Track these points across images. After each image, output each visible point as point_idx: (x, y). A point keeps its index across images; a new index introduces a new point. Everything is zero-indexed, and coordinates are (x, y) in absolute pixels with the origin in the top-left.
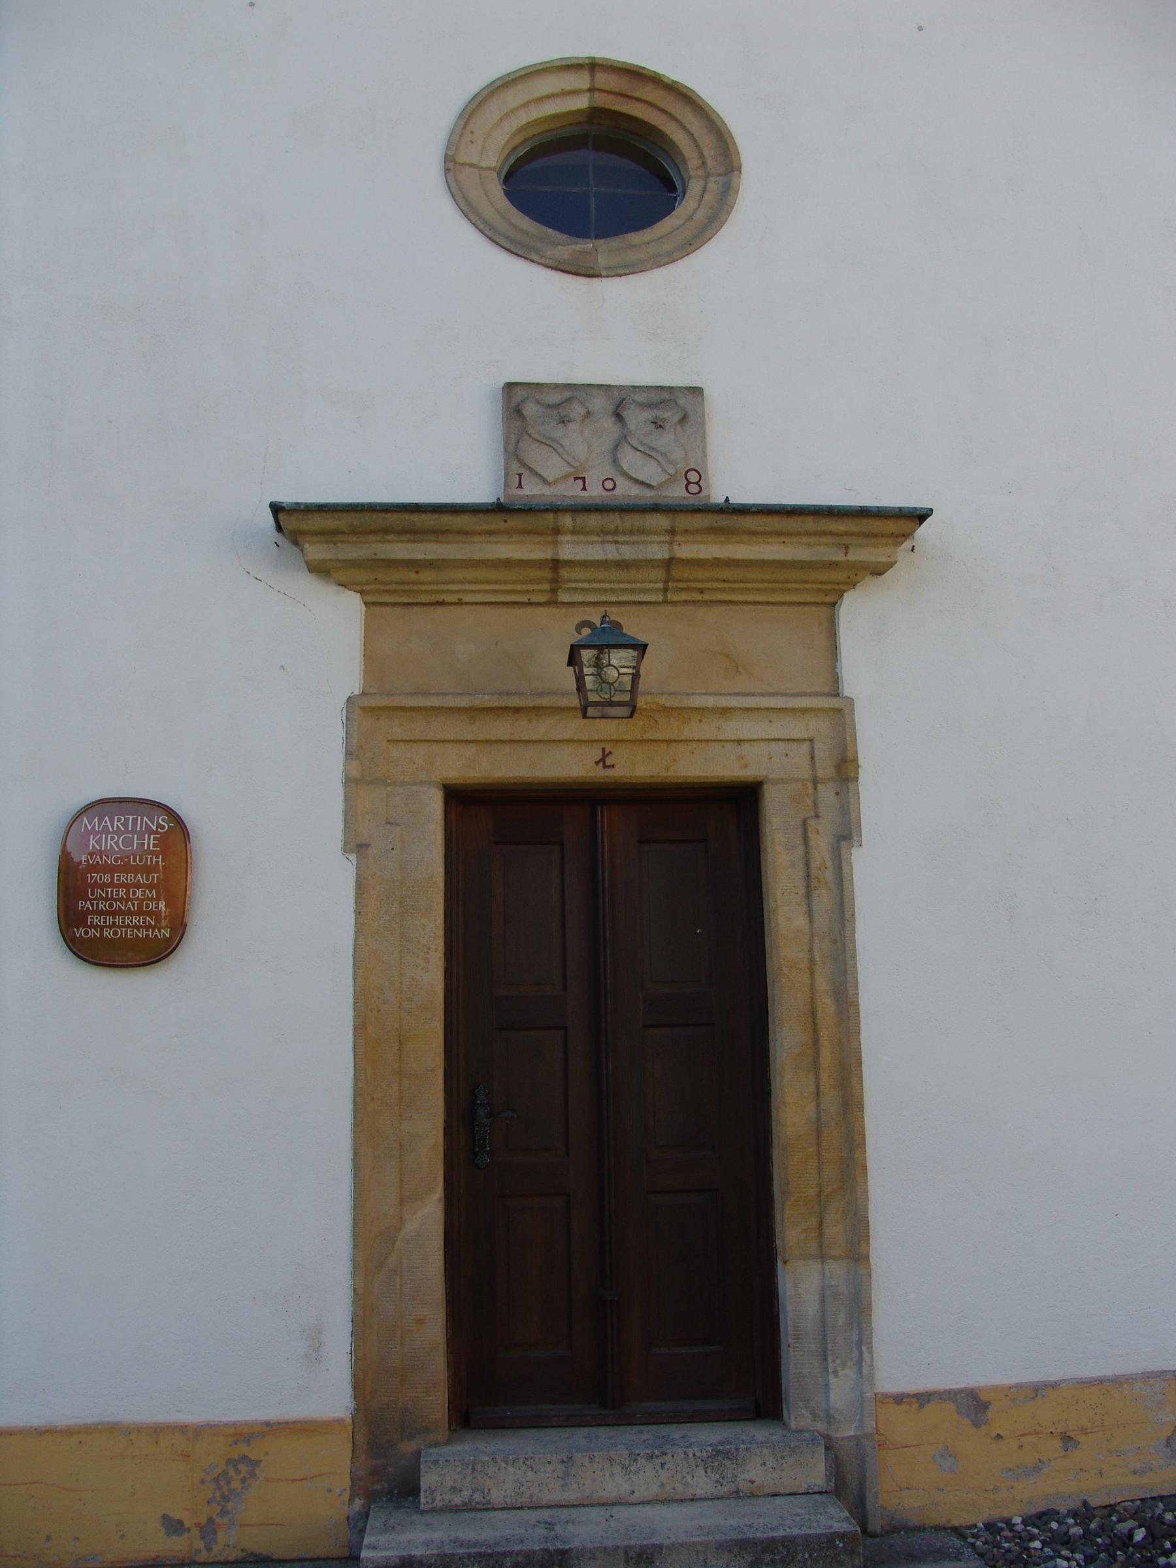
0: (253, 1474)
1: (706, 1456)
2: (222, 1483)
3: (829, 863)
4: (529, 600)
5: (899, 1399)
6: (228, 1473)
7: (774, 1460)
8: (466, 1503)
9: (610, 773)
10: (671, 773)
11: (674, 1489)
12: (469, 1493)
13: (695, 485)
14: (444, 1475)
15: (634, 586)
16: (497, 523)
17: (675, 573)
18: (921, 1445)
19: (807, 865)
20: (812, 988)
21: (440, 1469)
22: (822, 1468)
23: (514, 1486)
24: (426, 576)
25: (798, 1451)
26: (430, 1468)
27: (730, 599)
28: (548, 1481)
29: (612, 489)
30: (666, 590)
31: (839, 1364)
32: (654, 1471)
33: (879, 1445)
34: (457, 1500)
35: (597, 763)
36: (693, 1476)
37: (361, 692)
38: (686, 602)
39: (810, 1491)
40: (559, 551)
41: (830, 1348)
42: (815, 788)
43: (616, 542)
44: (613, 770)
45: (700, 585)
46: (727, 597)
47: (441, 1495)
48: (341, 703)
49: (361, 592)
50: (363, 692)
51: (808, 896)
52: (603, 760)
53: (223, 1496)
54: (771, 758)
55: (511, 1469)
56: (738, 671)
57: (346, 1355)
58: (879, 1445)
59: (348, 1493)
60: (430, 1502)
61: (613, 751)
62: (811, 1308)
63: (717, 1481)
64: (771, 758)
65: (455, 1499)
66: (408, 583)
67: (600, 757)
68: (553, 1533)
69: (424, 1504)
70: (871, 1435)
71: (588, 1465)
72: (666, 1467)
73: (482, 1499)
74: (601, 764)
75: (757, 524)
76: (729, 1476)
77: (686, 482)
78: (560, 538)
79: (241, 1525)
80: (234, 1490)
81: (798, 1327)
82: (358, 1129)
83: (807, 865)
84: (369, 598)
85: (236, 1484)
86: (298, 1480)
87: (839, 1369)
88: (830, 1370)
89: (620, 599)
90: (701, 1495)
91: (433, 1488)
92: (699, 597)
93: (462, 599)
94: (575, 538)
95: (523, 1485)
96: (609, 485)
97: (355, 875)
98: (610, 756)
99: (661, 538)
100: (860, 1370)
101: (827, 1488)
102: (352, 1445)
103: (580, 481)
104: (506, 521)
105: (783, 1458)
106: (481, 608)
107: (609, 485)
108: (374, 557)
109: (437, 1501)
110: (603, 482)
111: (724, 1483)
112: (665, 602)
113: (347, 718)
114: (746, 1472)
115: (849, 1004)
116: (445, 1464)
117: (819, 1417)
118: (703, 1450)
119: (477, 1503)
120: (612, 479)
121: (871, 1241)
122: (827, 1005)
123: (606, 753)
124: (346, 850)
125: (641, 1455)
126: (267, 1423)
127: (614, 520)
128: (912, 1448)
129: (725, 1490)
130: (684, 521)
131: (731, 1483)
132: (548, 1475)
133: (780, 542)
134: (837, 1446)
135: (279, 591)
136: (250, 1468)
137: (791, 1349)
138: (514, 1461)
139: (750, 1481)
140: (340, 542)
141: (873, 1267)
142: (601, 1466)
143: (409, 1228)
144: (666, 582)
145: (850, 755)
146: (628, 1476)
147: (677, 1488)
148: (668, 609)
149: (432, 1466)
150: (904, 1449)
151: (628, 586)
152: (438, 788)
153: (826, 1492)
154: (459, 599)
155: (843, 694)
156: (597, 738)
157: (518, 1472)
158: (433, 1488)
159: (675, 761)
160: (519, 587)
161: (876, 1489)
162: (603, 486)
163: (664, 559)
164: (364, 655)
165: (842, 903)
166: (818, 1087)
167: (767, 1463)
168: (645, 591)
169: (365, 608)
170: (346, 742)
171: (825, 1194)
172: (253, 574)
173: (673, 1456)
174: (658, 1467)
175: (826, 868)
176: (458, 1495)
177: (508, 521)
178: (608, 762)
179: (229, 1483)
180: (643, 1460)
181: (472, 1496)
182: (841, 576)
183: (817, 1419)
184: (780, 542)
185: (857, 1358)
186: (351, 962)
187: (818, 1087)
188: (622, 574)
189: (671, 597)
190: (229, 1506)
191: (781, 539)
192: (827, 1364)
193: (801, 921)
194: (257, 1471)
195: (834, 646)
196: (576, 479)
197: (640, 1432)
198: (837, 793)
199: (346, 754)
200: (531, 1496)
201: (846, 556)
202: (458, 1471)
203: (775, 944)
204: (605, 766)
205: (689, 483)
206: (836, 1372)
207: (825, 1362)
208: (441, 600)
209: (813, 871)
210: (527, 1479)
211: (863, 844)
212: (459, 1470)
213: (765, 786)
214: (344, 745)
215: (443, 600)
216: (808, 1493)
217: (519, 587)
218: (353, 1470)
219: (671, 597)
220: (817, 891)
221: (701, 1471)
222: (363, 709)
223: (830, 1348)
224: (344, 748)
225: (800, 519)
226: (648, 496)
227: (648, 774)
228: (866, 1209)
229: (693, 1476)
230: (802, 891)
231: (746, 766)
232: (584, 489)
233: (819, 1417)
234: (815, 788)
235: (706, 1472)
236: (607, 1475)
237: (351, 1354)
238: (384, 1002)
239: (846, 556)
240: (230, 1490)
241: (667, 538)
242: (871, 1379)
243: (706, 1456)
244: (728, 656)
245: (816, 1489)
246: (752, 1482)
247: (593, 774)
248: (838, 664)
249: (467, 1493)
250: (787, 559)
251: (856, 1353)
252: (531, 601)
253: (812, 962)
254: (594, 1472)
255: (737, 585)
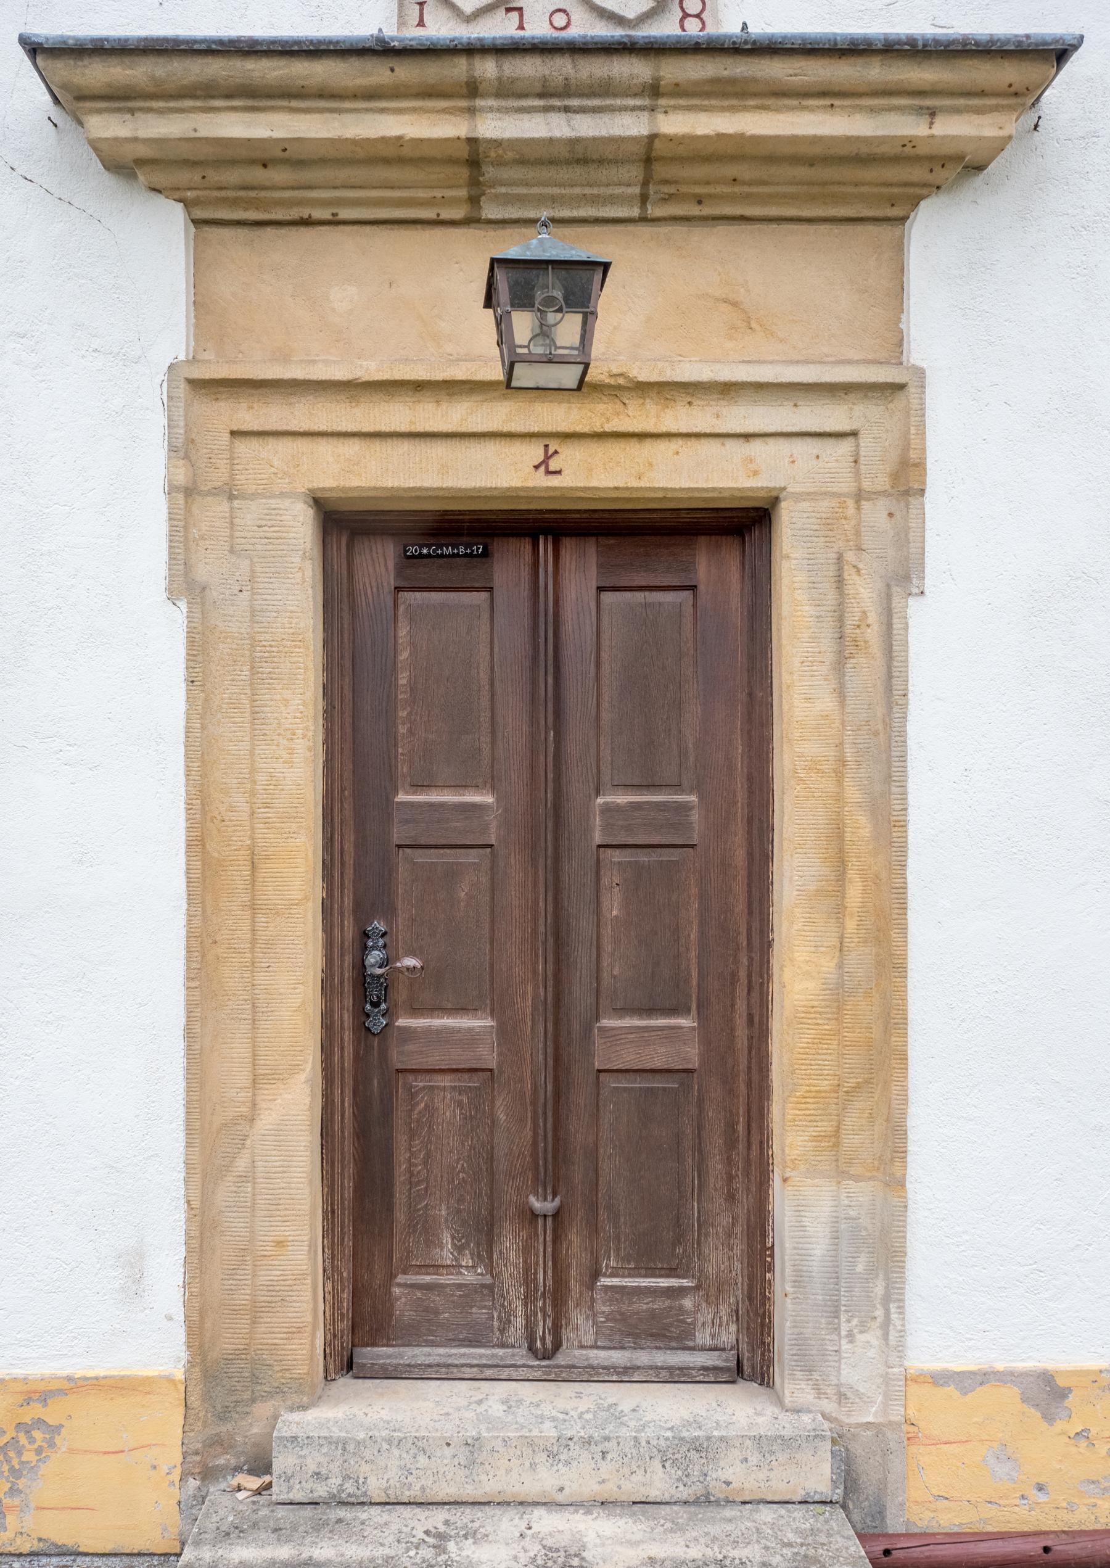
0: (52, 1444)
1: (664, 1445)
2: (12, 1454)
3: (873, 618)
4: (438, 215)
5: (940, 1379)
6: (18, 1442)
7: (760, 1457)
8: (334, 1496)
9: (554, 482)
10: (643, 484)
11: (619, 1487)
12: (339, 1481)
13: (698, 12)
14: (304, 1457)
15: (595, 191)
16: (378, 73)
17: (661, 171)
18: (967, 1441)
19: (841, 620)
20: (839, 798)
21: (299, 1449)
22: (826, 1468)
23: (400, 1474)
24: (278, 175)
25: (793, 1444)
26: (286, 1447)
27: (743, 213)
28: (446, 1469)
29: (559, 10)
30: (644, 199)
31: (856, 1325)
32: (592, 1462)
33: (909, 1439)
34: (321, 1491)
35: (536, 467)
36: (646, 1471)
37: (191, 357)
38: (675, 219)
39: (809, 1500)
40: (479, 126)
41: (843, 1303)
42: (858, 508)
43: (567, 109)
44: (559, 476)
45: (698, 190)
46: (738, 211)
47: (300, 1482)
48: (161, 375)
49: (187, 204)
50: (194, 357)
51: (840, 664)
52: (545, 462)
53: (12, 1469)
54: (793, 462)
55: (396, 1452)
56: (751, 328)
57: (178, 1288)
58: (909, 1439)
59: (178, 1471)
60: (285, 1491)
61: (559, 450)
62: (819, 1248)
63: (679, 1480)
64: (793, 462)
65: (319, 1489)
66: (253, 188)
67: (542, 458)
68: (443, 1557)
69: (277, 1495)
70: (899, 1424)
71: (501, 1450)
72: (609, 1456)
73: (356, 1491)
74: (542, 469)
75: (791, 72)
76: (695, 1473)
77: (681, 14)
78: (479, 103)
79: (38, 1508)
80: (28, 1462)
81: (801, 1271)
82: (193, 984)
83: (841, 620)
84: (200, 214)
85: (29, 1456)
86: (113, 1453)
87: (855, 1331)
88: (843, 1333)
89: (575, 213)
90: (656, 1497)
91: (289, 1473)
92: (695, 210)
93: (337, 214)
94: (503, 103)
95: (411, 1474)
96: (560, 20)
97: (185, 628)
98: (556, 457)
99: (638, 102)
100: (886, 1336)
101: (832, 1496)
102: (182, 1409)
103: (515, 15)
104: (392, 70)
105: (772, 1453)
106: (368, 229)
107: (560, 20)
108: (193, 135)
109: (295, 1491)
110: (551, 15)
111: (689, 1483)
112: (644, 219)
113: (168, 397)
114: (720, 1469)
115: (893, 823)
116: (306, 1442)
117: (825, 1393)
118: (661, 1438)
119: (349, 1495)
120: (559, 10)
121: (909, 1159)
122: (860, 826)
123: (550, 453)
124: (172, 596)
125: (574, 1440)
126: (69, 1379)
127: (562, 68)
128: (955, 1445)
129: (690, 1492)
130: (674, 70)
131: (698, 1483)
132: (445, 1462)
133: (825, 107)
134: (849, 1436)
135: (60, 199)
136: (48, 1436)
137: (788, 1300)
138: (400, 1441)
139: (724, 1482)
140: (141, 109)
141: (910, 1195)
142: (519, 1452)
143: (267, 1120)
144: (645, 184)
145: (913, 455)
146: (555, 1468)
147: (623, 1486)
148: (645, 230)
149: (289, 1445)
150: (943, 1446)
151: (588, 191)
152: (305, 502)
153: (831, 1502)
154: (333, 214)
155: (908, 361)
156: (536, 429)
157: (404, 1455)
158: (289, 1473)
159: (651, 464)
160: (421, 194)
161: (901, 1499)
162: (551, 24)
163: (642, 137)
164: (195, 302)
165: (890, 677)
166: (842, 938)
167: (750, 1459)
168: (612, 200)
169: (194, 230)
170: (169, 433)
171: (845, 1089)
172: (20, 171)
173: (618, 1443)
174: (598, 1456)
175: (868, 626)
176: (323, 1483)
177: (396, 69)
178: (553, 465)
179: (20, 1454)
180: (577, 1447)
181: (341, 1485)
182: (917, 173)
183: (822, 1396)
184: (825, 107)
185: (883, 1318)
186: (182, 750)
187: (842, 938)
188: (578, 173)
189: (653, 211)
190: (21, 1483)
191: (827, 102)
192: (839, 1324)
193: (826, 703)
194: (58, 1440)
195: (900, 287)
196: (508, 10)
197: (579, 1395)
198: (891, 515)
199: (169, 450)
200: (423, 1489)
201: (930, 128)
202: (323, 1451)
203: (787, 734)
204: (548, 472)
205: (686, 15)
206: (850, 1336)
207: (836, 1321)
208: (306, 216)
209: (848, 630)
210: (418, 1466)
211: (927, 591)
212: (324, 1450)
213: (783, 505)
214: (166, 437)
215: (310, 216)
216: (806, 1502)
217: (421, 194)
218: (186, 1441)
219: (653, 211)
220: (852, 661)
221: (657, 1464)
222: (191, 382)
223: (843, 1303)
224: (166, 443)
225: (860, 61)
226: (616, 33)
227: (611, 484)
228: (904, 1114)
229: (646, 1471)
230: (829, 658)
231: (756, 473)
232: (521, 27)
233: (825, 1393)
234: (858, 508)
235: (664, 1466)
236: (527, 1465)
237: (184, 1287)
238: (231, 809)
239: (930, 128)
240: (22, 1463)
241: (646, 102)
242: (900, 1349)
243: (664, 1445)
244: (735, 304)
245: (817, 1498)
246: (728, 1483)
247: (530, 484)
248: (904, 317)
249: (335, 1482)
250: (835, 134)
251: (879, 1313)
252: (441, 217)
253: (842, 761)
254: (509, 1460)
255: (754, 190)
